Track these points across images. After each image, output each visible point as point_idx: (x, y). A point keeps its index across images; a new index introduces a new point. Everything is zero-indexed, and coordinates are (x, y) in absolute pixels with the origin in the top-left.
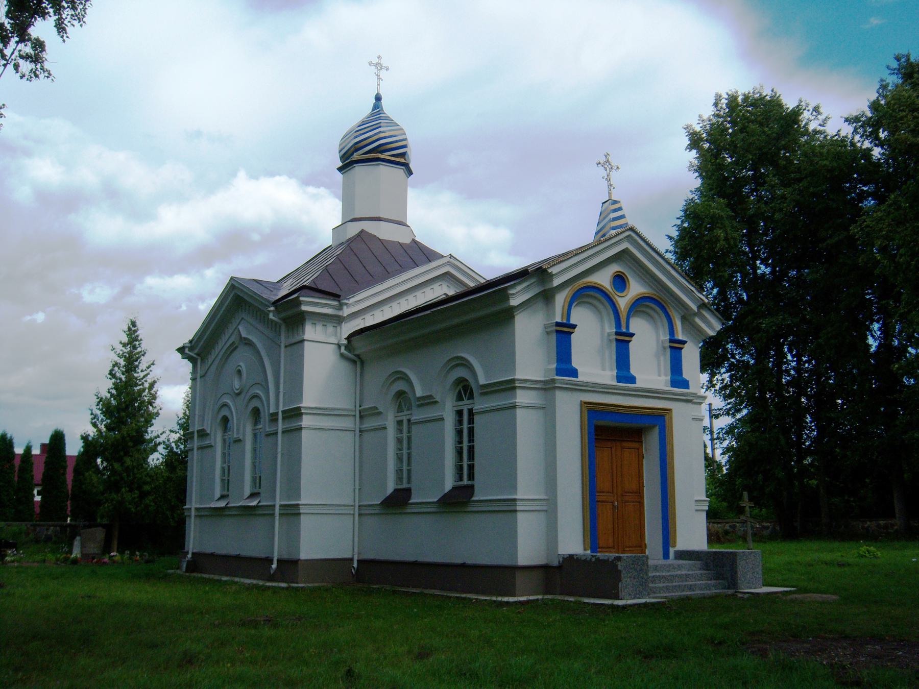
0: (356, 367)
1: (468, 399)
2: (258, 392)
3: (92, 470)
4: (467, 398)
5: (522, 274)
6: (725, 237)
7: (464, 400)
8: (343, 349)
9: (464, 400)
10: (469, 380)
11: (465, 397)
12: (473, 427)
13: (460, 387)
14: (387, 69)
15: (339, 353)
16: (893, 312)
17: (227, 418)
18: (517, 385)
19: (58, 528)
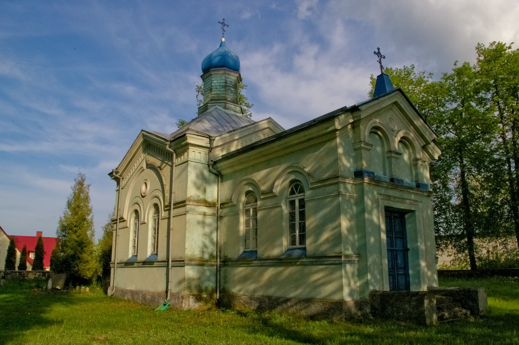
0: (8, 236)
1: (298, 194)
2: (158, 194)
3: (11, 258)
4: (298, 192)
5: (344, 110)
6: (475, 300)
7: (295, 194)
8: (211, 167)
9: (295, 194)
10: (58, 275)
11: (297, 192)
12: (305, 210)
13: (292, 185)
14: (384, 57)
15: (208, 170)
16: (507, 93)
17: (137, 211)
18: (340, 180)
19: (41, 273)
